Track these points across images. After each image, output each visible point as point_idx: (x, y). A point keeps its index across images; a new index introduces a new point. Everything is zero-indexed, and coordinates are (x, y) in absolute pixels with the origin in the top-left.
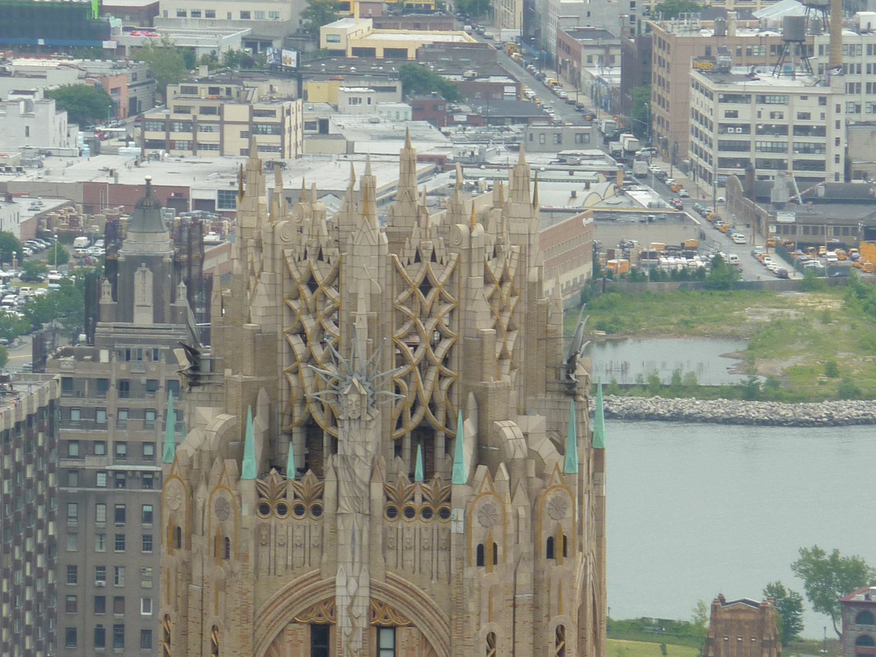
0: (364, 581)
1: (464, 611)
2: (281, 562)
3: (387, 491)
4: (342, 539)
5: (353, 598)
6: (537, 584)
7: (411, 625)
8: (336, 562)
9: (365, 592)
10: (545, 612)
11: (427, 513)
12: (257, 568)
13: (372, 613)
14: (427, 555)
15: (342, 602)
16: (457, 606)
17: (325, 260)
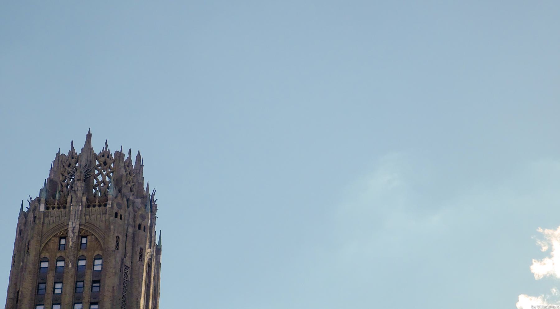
0: (78, 223)
1: (110, 228)
2: (51, 221)
3: (87, 199)
4: (71, 213)
5: (74, 228)
6: (134, 234)
7: (93, 235)
8: (69, 219)
9: (78, 226)
10: (137, 243)
11: (100, 206)
12: (43, 223)
13: (79, 232)
14: (99, 216)
15: (70, 228)
16: (108, 228)
17: (119, 217)
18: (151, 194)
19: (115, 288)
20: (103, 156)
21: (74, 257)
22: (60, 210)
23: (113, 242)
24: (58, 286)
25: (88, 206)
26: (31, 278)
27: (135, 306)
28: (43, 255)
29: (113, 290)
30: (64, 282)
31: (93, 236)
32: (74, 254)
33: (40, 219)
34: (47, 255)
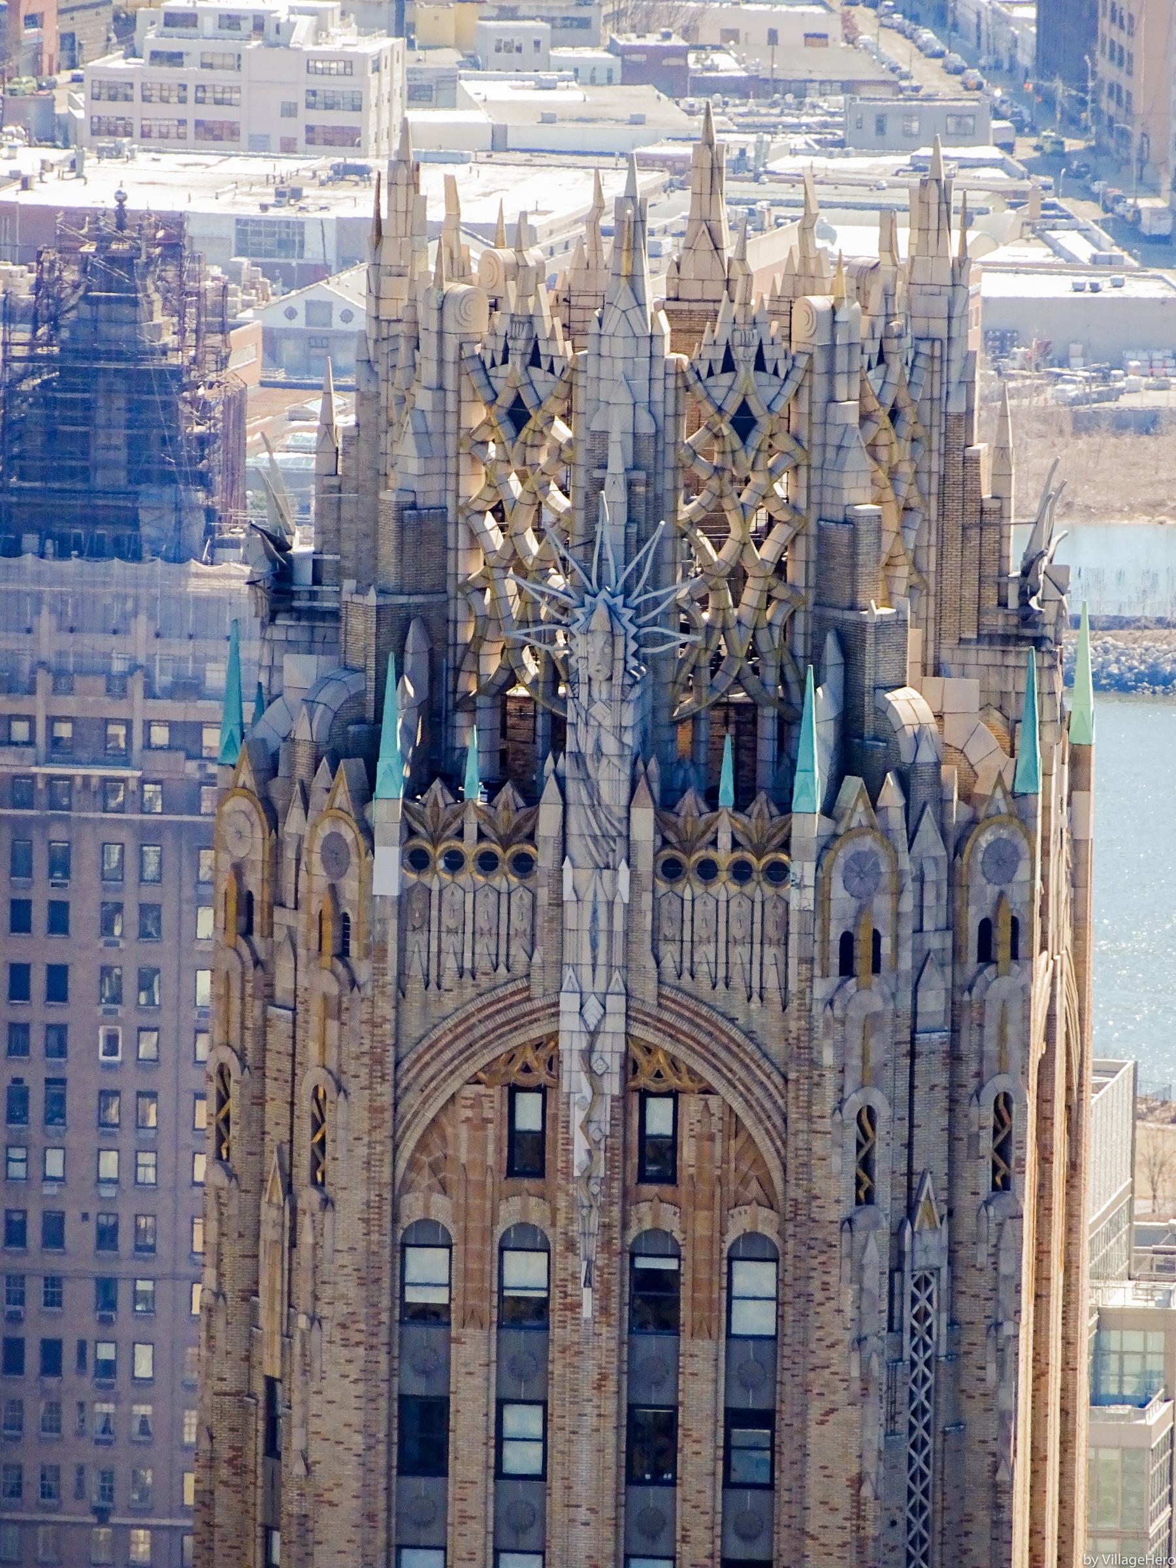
2: (450, 963)
9: (615, 1023)
13: (630, 1067)
15: (571, 1043)
18: (1015, 573)
19: (867, 1491)
20: (729, 365)
21: (606, 1245)
22: (499, 881)
23: (836, 1161)
24: (522, 1420)
25: (671, 870)
26: (354, 1372)
27: (983, 1517)
28: (413, 1208)
29: (858, 1502)
30: (554, 1397)
31: (713, 1101)
32: (606, 1227)
33: (375, 952)
34: (441, 1209)
